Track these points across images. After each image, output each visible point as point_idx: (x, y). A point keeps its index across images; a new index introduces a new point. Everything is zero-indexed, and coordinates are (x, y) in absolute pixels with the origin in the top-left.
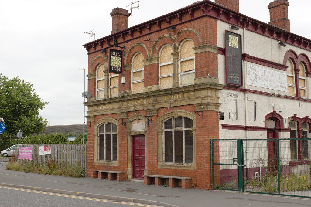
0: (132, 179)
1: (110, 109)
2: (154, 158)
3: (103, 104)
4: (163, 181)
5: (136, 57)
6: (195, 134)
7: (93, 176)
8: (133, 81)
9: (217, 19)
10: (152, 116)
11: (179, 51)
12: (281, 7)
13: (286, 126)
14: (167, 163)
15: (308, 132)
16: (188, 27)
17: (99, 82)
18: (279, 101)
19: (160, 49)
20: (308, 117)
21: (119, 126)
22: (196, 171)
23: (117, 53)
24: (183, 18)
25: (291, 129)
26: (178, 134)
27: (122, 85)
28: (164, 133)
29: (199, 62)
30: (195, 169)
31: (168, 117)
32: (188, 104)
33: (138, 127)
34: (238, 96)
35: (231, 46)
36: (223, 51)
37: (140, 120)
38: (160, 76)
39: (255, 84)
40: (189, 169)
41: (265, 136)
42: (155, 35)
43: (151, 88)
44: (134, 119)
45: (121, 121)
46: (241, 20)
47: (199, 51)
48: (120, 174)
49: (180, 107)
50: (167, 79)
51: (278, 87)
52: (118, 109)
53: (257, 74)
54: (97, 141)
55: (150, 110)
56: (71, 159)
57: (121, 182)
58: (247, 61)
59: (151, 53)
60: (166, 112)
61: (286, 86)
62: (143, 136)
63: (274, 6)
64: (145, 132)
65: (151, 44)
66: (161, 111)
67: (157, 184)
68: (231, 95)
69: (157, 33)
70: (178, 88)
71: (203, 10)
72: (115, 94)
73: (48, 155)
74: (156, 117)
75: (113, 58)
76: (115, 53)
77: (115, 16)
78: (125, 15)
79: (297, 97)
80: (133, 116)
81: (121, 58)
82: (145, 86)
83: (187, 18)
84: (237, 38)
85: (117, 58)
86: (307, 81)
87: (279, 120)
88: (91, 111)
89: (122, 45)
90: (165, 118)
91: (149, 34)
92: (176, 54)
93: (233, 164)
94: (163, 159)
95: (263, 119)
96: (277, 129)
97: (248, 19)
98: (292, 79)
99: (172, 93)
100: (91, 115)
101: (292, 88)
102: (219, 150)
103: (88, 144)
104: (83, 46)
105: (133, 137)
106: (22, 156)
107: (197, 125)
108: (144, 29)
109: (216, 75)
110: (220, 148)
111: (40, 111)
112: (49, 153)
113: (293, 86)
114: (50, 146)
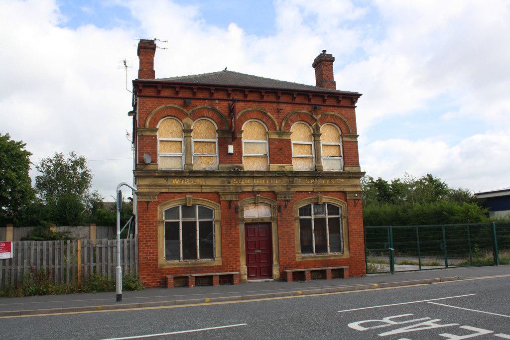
3: (173, 176)
26: (320, 222)
32: (337, 190)
33: (255, 212)
40: (341, 258)
43: (284, 167)
49: (326, 193)
52: (218, 187)
54: (162, 231)
70: (192, 172)
104: (361, 95)
105: (246, 224)
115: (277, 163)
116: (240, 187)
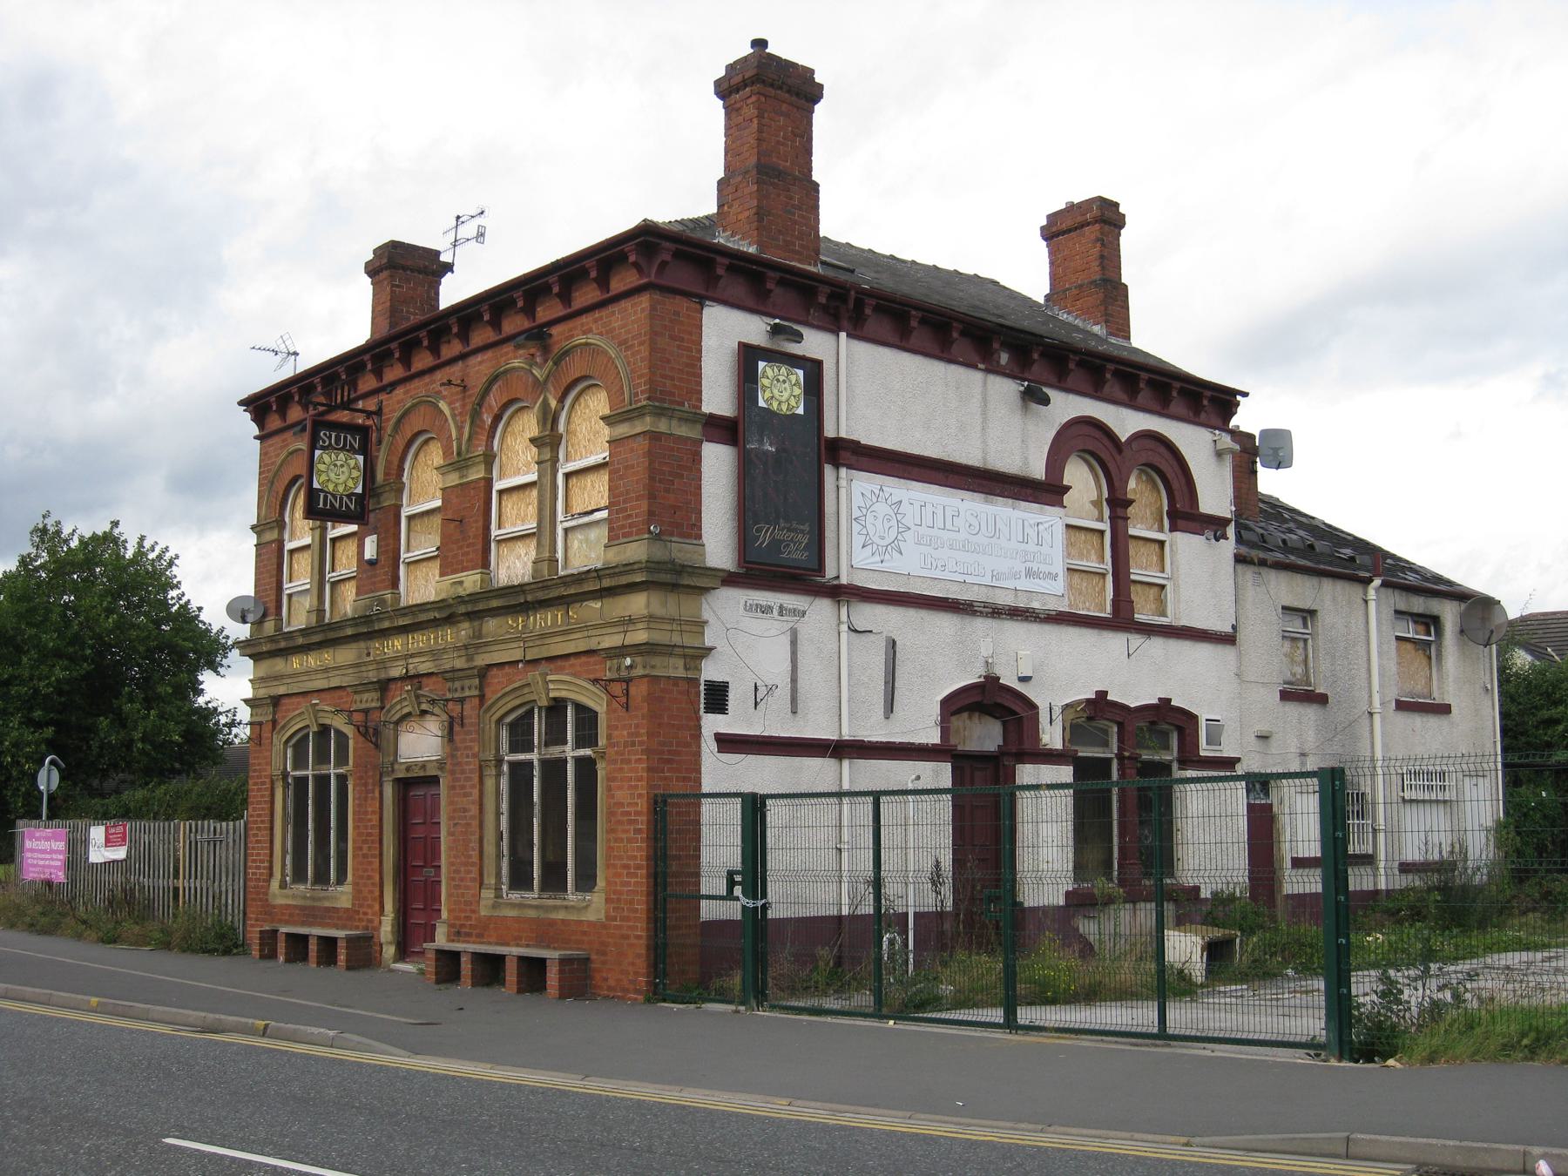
0: (394, 962)
1: (326, 670)
2: (469, 872)
4: (490, 969)
5: (422, 455)
6: (604, 772)
7: (261, 950)
8: (408, 551)
9: (701, 300)
10: (462, 700)
11: (561, 428)
12: (1092, 232)
13: (1052, 736)
14: (515, 896)
15: (1175, 766)
16: (590, 331)
17: (296, 556)
18: (1015, 632)
19: (497, 419)
20: (1106, 693)
21: (356, 743)
22: (604, 926)
23: (345, 438)
24: (573, 295)
25: (1080, 754)
27: (368, 567)
28: (505, 768)
29: (621, 478)
30: (602, 916)
31: (518, 702)
32: (582, 647)
34: (804, 613)
35: (767, 411)
36: (724, 430)
37: (428, 717)
38: (495, 532)
39: (895, 564)
41: (946, 780)
42: (480, 363)
43: (461, 583)
44: (406, 710)
45: (358, 717)
46: (822, 300)
47: (623, 430)
48: (349, 939)
49: (559, 663)
50: (519, 544)
51: (1016, 576)
52: (351, 671)
53: (907, 521)
55: (451, 675)
56: (193, 880)
57: (351, 974)
58: (850, 467)
59: (466, 435)
60: (510, 682)
61: (1059, 567)
62: (434, 781)
63: (1064, 227)
64: (441, 764)
65: (467, 401)
66: (496, 677)
67: (469, 981)
68: (766, 610)
69: (489, 354)
71: (635, 265)
72: (349, 602)
73: (118, 861)
74: (477, 701)
75: (326, 458)
76: (333, 435)
77: (385, 274)
78: (424, 271)
79: (1121, 620)
80: (400, 701)
81: (361, 458)
82: (442, 574)
83: (586, 295)
84: (801, 373)
85: (342, 456)
86: (1172, 550)
87: (1015, 713)
88: (262, 678)
89: (371, 404)
90: (509, 706)
91: (463, 357)
92: (549, 442)
93: (730, 896)
94: (501, 878)
95: (936, 710)
96: (1009, 754)
97: (857, 292)
98: (1095, 539)
99: (526, 602)
100: (262, 693)
101: (1096, 579)
102: (698, 839)
103: (252, 816)
104: (241, 403)
106: (35, 866)
107: (609, 737)
108: (445, 339)
109: (692, 530)
110: (704, 829)
111: (207, 678)
112: (120, 853)
113: (1104, 571)
114: (125, 826)
115: (573, 575)
116: (382, 664)
